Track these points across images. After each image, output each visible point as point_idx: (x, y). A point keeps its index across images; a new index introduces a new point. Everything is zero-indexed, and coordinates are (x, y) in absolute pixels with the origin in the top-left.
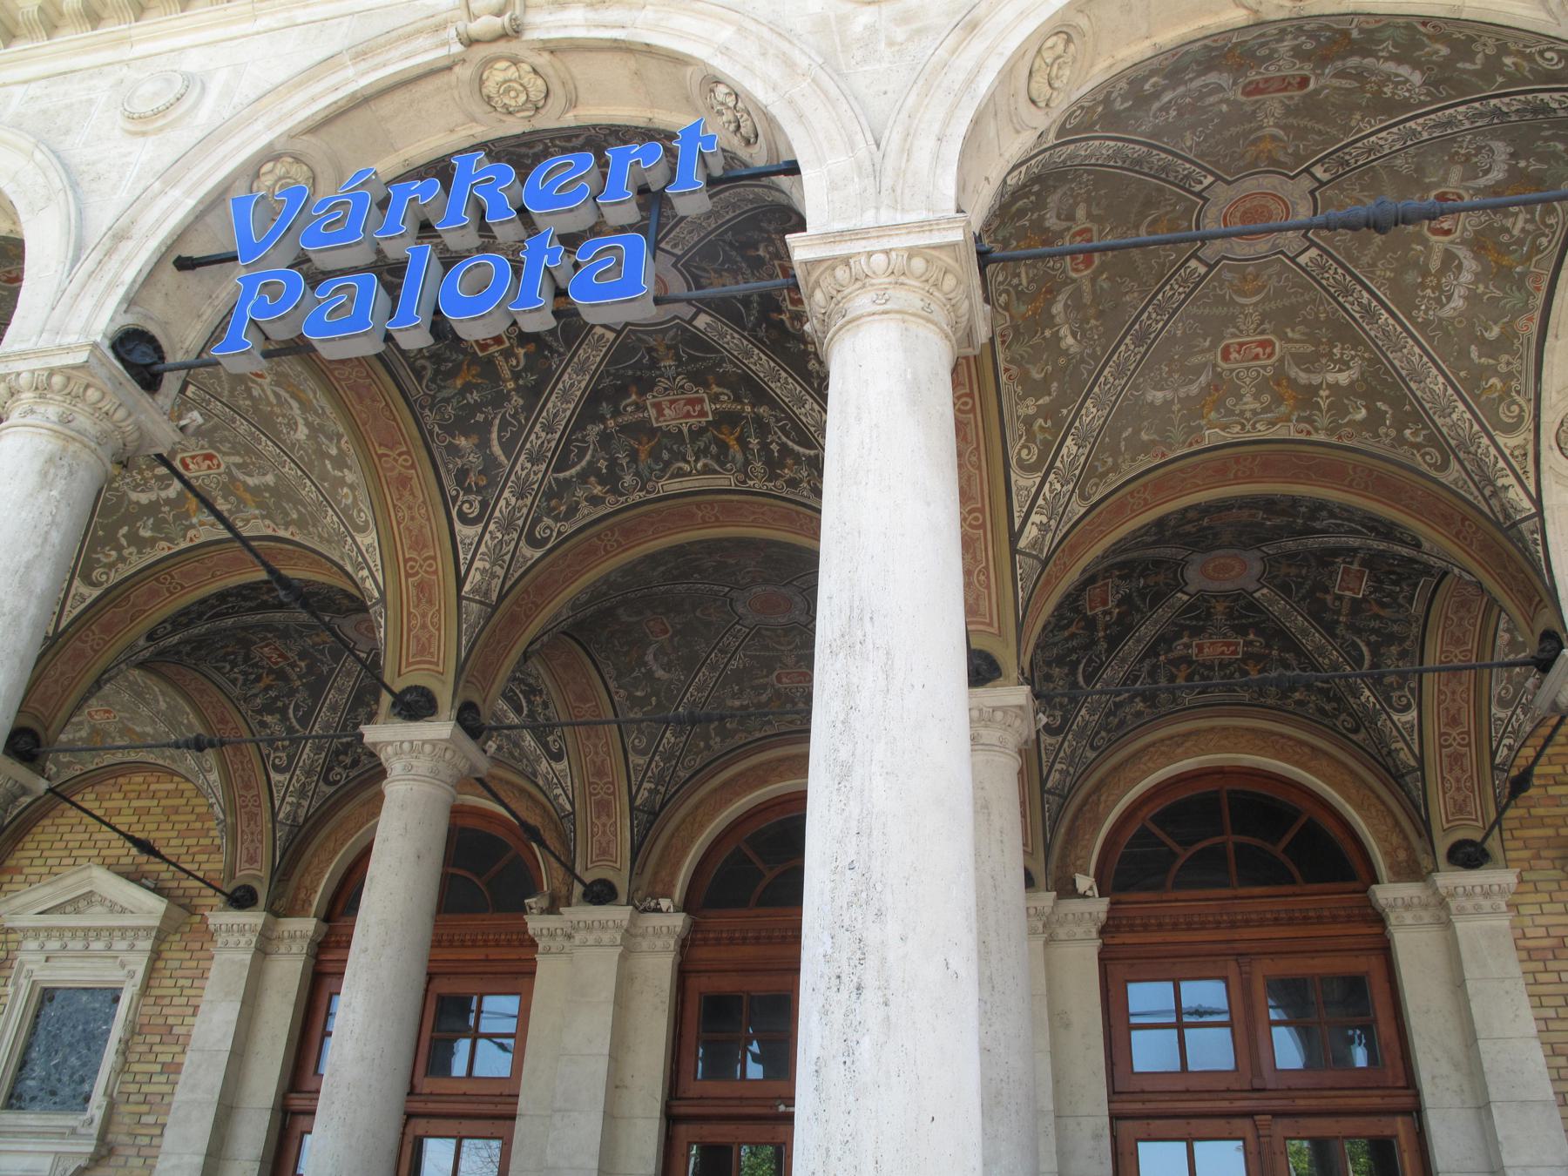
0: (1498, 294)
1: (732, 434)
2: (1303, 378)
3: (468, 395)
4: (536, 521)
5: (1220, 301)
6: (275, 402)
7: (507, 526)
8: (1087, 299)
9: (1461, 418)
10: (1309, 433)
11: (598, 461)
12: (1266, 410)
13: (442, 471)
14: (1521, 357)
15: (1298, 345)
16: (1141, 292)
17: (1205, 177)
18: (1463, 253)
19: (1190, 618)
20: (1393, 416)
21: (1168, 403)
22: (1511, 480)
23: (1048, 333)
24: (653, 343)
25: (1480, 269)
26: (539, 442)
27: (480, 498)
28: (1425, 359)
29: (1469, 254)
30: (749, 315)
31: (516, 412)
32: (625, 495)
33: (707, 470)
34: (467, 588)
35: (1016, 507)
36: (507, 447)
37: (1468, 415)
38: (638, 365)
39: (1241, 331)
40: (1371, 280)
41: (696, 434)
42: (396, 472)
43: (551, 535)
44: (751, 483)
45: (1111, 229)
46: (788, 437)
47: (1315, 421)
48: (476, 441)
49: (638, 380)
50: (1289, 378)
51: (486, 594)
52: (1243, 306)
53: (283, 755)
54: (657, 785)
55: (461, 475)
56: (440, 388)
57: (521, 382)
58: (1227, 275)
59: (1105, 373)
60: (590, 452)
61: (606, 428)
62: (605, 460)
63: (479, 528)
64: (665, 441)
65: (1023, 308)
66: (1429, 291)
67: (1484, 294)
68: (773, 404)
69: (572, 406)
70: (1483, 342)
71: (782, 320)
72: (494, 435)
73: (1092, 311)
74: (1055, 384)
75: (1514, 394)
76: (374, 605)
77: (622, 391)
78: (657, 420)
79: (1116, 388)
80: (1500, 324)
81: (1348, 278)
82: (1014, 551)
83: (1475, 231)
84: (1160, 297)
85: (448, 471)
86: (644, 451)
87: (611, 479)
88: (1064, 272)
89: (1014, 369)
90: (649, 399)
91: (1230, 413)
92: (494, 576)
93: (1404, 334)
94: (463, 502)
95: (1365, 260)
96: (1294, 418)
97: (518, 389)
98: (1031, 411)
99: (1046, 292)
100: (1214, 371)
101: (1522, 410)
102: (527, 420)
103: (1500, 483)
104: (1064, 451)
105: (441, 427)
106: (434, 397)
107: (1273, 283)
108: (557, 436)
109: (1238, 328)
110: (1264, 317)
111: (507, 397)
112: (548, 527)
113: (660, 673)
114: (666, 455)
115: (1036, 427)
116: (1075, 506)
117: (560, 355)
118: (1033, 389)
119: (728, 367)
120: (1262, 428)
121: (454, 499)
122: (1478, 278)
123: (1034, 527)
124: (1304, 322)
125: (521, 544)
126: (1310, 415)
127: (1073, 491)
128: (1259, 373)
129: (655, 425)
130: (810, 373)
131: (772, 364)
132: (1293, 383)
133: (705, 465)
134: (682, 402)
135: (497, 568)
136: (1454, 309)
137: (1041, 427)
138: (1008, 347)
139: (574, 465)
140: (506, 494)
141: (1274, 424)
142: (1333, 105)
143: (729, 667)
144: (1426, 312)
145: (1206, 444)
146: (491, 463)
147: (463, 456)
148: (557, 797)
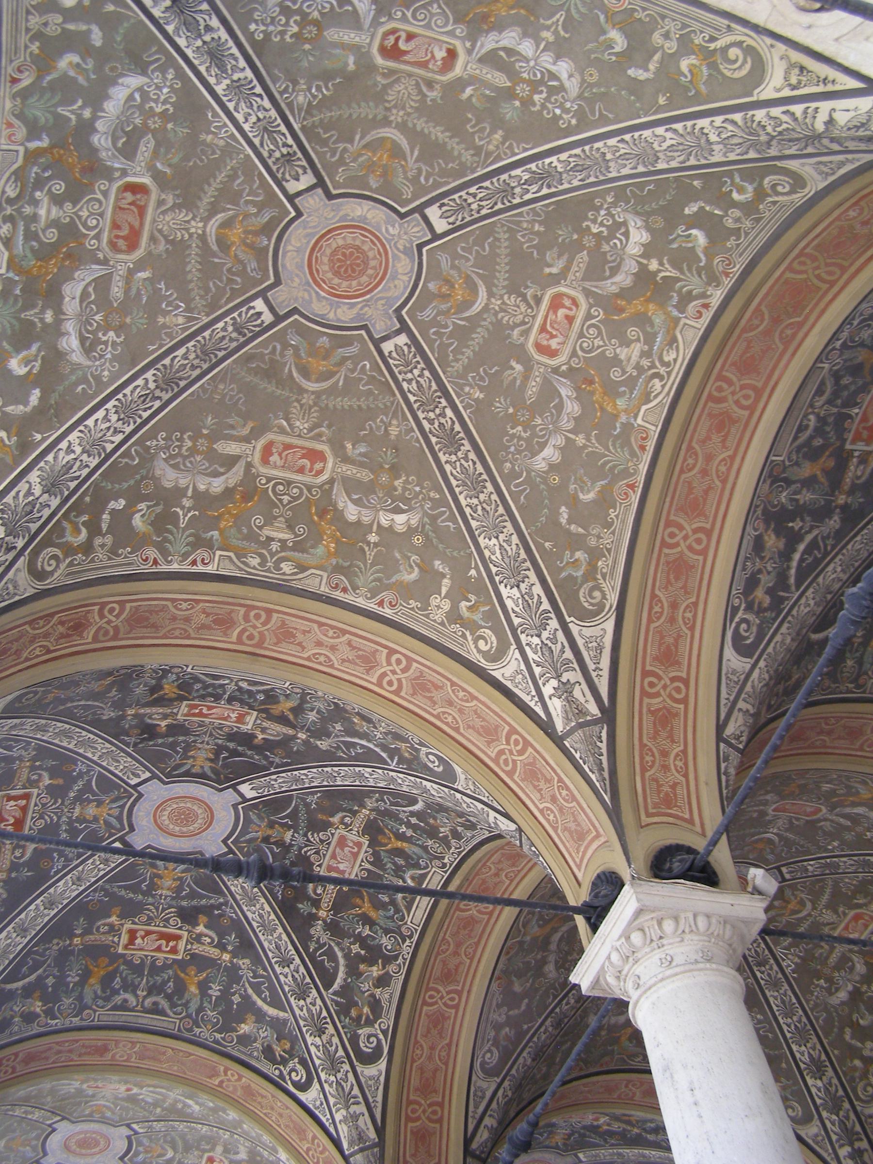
0: (561, 16)
2: (623, 279)
3: (210, 992)
4: (354, 1040)
5: (462, 334)
6: (849, 823)
7: (333, 1065)
8: (365, 475)
9: (720, 130)
10: (706, 306)
12: (650, 339)
13: (254, 1063)
14: (663, 17)
15: (574, 268)
16: (395, 415)
18: (489, 42)
19: (126, 888)
20: (708, 202)
21: (568, 448)
22: (825, 106)
23: (373, 538)
25: (519, 29)
27: (296, 1060)
28: (627, 137)
29: (493, 36)
30: (253, 758)
31: (254, 972)
32: (399, 954)
34: (345, 1145)
35: (526, 698)
36: (275, 1003)
37: (718, 120)
39: (523, 323)
40: (498, 159)
43: (379, 1041)
45: (287, 420)
47: (690, 292)
48: (253, 1018)
50: (617, 296)
52: (486, 308)
54: (851, 1144)
55: (268, 1052)
56: (186, 1005)
57: (230, 948)
58: (428, 314)
59: (463, 503)
60: (336, 949)
61: (324, 921)
63: (316, 1085)
65: (320, 550)
66: (536, 97)
67: (556, 33)
70: (627, 57)
72: (260, 1003)
73: (384, 478)
74: (437, 563)
75: (712, 46)
79: (489, 502)
80: (607, 27)
81: (487, 184)
82: (558, 740)
83: (456, 21)
84: (412, 399)
86: (366, 907)
87: (374, 954)
88: (309, 488)
89: (385, 595)
91: (631, 382)
92: (355, 1117)
93: (587, 148)
94: (290, 1074)
95: (467, 156)
96: (675, 313)
98: (446, 605)
99: (321, 517)
100: (563, 375)
101: (739, 44)
102: (265, 970)
103: (820, 127)
104: (509, 604)
105: (219, 1031)
106: (189, 1016)
107: (468, 267)
108: (297, 960)
109: (516, 325)
110: (514, 289)
111: (235, 968)
112: (369, 1036)
115: (465, 613)
116: (587, 632)
120: (673, 355)
121: (281, 1076)
122: (530, 31)
123: (554, 699)
124: (542, 249)
125: (359, 1069)
126: (679, 292)
128: (593, 325)
132: (623, 293)
134: (338, 850)
135: (353, 1108)
136: (571, 76)
137: (469, 608)
138: (355, 588)
139: (336, 969)
140: (309, 1040)
141: (674, 340)
142: (186, 158)
143: (788, 971)
144: (566, 111)
145: (655, 432)
146: (277, 1025)
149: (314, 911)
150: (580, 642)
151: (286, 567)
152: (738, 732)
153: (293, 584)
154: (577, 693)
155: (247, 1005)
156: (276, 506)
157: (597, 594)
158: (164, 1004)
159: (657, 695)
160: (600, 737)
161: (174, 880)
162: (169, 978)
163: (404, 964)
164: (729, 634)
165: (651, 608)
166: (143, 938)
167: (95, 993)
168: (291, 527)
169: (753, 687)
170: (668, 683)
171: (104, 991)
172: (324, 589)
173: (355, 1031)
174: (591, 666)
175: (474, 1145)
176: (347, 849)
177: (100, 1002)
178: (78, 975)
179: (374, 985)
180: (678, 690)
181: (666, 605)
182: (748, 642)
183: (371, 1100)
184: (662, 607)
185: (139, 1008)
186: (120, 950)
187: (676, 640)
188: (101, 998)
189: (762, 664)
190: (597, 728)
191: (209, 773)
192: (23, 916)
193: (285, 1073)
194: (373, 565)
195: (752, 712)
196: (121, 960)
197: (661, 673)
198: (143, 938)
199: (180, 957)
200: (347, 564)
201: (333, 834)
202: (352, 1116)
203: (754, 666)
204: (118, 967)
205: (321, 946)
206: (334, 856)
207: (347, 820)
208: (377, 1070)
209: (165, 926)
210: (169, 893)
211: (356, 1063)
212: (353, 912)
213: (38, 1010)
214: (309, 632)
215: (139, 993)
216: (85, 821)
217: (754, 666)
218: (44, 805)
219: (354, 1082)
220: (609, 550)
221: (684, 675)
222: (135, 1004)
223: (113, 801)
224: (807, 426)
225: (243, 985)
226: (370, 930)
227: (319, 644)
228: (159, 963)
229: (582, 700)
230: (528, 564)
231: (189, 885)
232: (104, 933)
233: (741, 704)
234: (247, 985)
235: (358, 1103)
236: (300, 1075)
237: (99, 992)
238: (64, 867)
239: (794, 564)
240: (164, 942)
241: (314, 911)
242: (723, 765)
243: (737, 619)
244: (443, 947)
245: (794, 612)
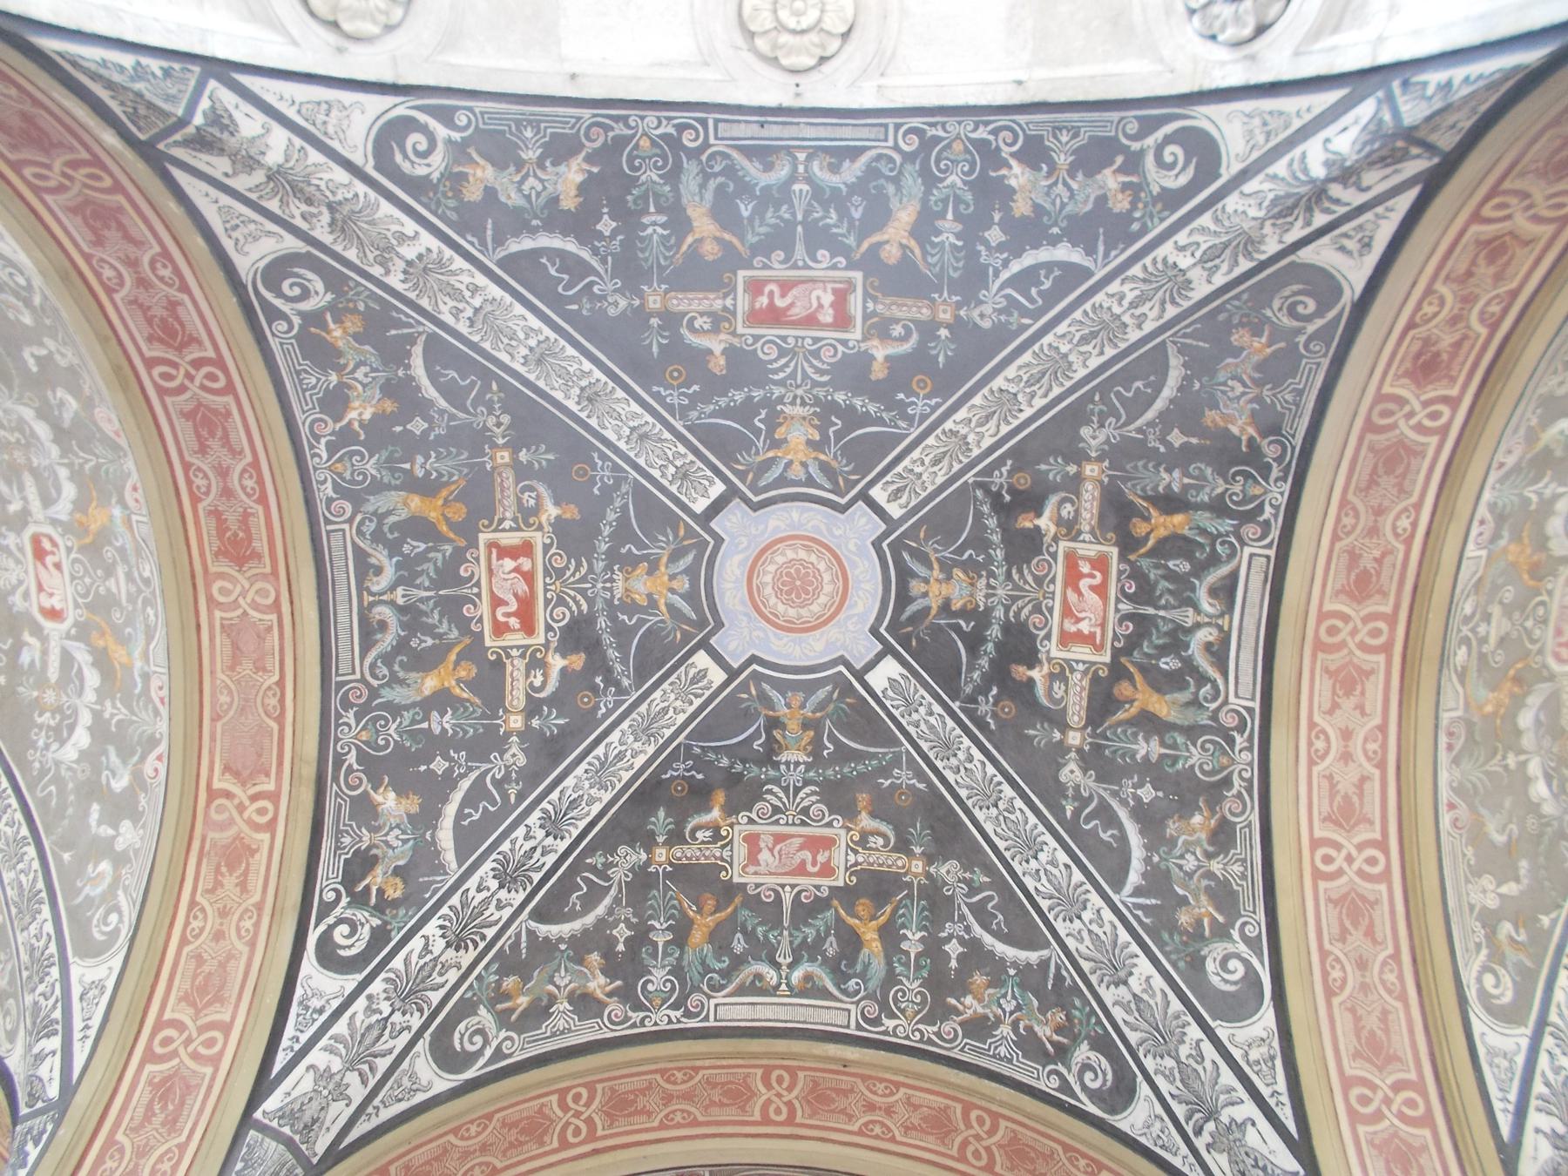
1: (873, 918)
3: (435, 715)
4: (466, 1008)
24: (782, 711)
26: (528, 846)
27: (376, 922)
30: (971, 669)
31: (507, 778)
33: (810, 989)
34: (272, 1103)
36: (467, 839)
38: (741, 752)
41: (806, 910)
42: (232, 832)
43: (480, 1052)
46: (985, 926)
48: (415, 809)
49: (732, 780)
51: (308, 1128)
56: (394, 680)
57: (535, 723)
60: (607, 901)
61: (649, 862)
62: (629, 926)
63: (350, 982)
64: (745, 913)
68: (971, 856)
69: (607, 797)
71: (1031, 681)
72: (451, 809)
77: (699, 795)
78: (851, 285)
86: (703, 924)
88: (1540, 652)
89: (1463, 811)
90: (740, 828)
92: (340, 1093)
94: (340, 921)
97: (526, 734)
98: (1492, 903)
102: (521, 797)
105: (362, 757)
106: (374, 693)
108: (562, 846)
112: (481, 1032)
114: (739, 944)
117: (621, 691)
118: (1496, 862)
119: (904, 776)
121: (326, 909)
130: (1061, 789)
131: (991, 770)
133: (808, 978)
134: (797, 842)
135: (352, 1078)
139: (573, 916)
140: (431, 928)
146: (425, 858)
147: (376, 830)
149: (661, 839)
151: (1462, 653)
153: (1445, 671)
155: (434, 792)
156: (1523, 611)
158: (387, 641)
161: (649, 596)
162: (440, 636)
163: (634, 1026)
164: (402, 107)
166: (517, 570)
167: (389, 513)
168: (1502, 641)
171: (394, 527)
172: (1445, 717)
173: (480, 1001)
177: (370, 527)
178: (428, 474)
179: (572, 992)
183: (376, 1102)
185: (368, 599)
186: (483, 538)
188: (380, 524)
191: (911, 609)
192: (570, 351)
193: (338, 911)
194: (1487, 773)
196: (462, 543)
198: (517, 570)
199: (488, 642)
200: (1478, 738)
201: (829, 824)
202: (339, 1085)
204: (449, 541)
205: (1086, 802)
206: (779, 838)
208: (431, 1078)
209: (547, 602)
210: (618, 593)
211: (427, 1035)
212: (686, 903)
213: (353, 415)
214: (1363, 714)
215: (400, 591)
216: (772, 427)
218: (816, 354)
219: (396, 1052)
222: (375, 589)
223: (825, 468)
225: (470, 769)
226: (667, 943)
227: (1347, 735)
228: (467, 610)
231: (642, 622)
232: (519, 500)
234: (473, 775)
235: (364, 1082)
236: (350, 944)
237: (392, 519)
238: (670, 409)
240: (513, 607)
241: (661, 839)
244: (679, 1075)
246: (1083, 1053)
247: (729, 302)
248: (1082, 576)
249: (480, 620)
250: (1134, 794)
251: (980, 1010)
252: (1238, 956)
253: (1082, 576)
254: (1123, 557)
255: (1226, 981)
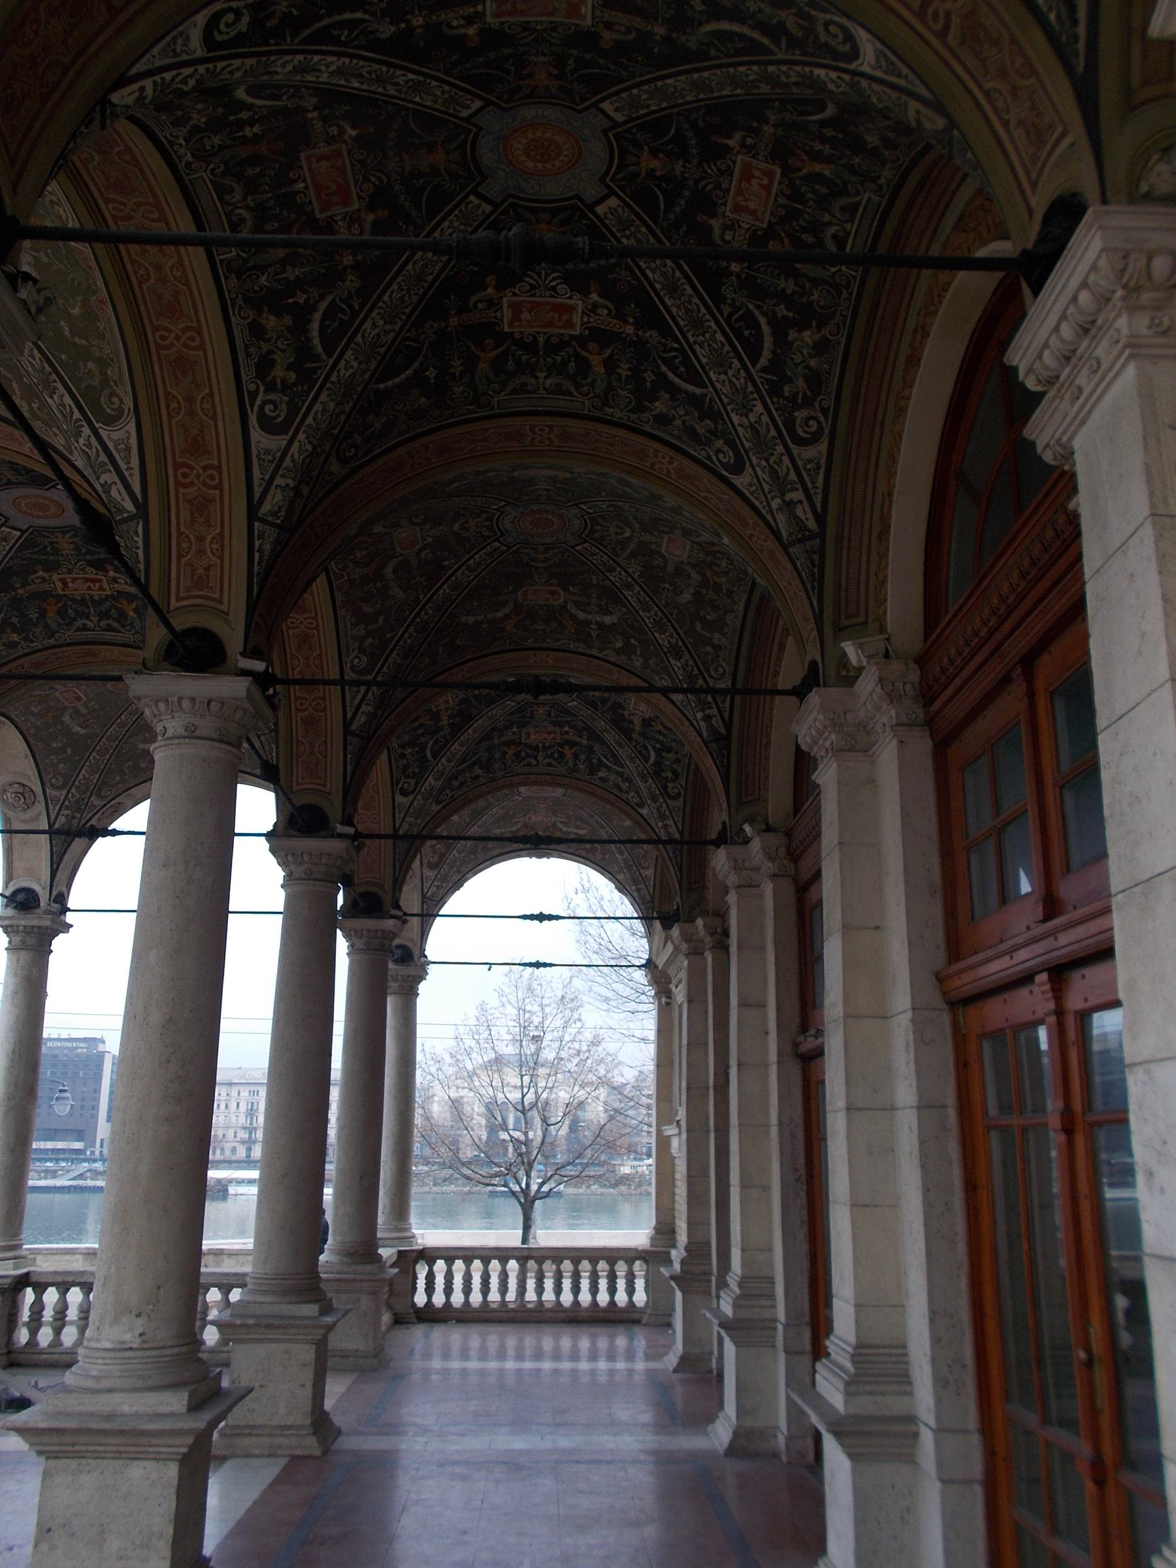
11: (427, 370)
17: (473, 101)
34: (785, 536)
36: (693, 377)
42: (175, 349)
43: (819, 423)
44: (610, 411)
53: (632, 794)
60: (757, 313)
61: (738, 276)
76: (124, 520)
85: (248, 355)
92: (74, 817)
94: (264, 403)
98: (363, 633)
102: (362, 306)
105: (632, 411)
113: (608, 620)
116: (116, 436)
121: (253, 395)
127: (95, 432)
129: (506, 329)
148: (107, 487)
150: (111, 445)
152: (276, 508)
154: (114, 493)
157: (115, 399)
159: (192, 484)
160: (136, 532)
164: (253, 419)
165: (168, 406)
169: (293, 461)
170: (201, 471)
174: (123, 466)
175: (354, 727)
176: (754, 181)
180: (212, 477)
181: (181, 400)
182: (279, 420)
184: (178, 402)
187: (201, 431)
189: (301, 436)
190: (133, 524)
193: (712, 454)
195: (292, 485)
197: (192, 463)
199: (578, 333)
203: (291, 442)
205: (736, 309)
207: (749, 141)
211: (791, 446)
217: (291, 442)
220: (112, 360)
221: (215, 462)
224: (558, 385)
229: (119, 498)
230: (54, 376)
233: (279, 481)
239: (315, 333)
242: (257, 543)
243: (258, 403)
245: (333, 378)
246: (719, 443)
247: (480, 8)
248: (752, 177)
249: (310, 203)
250: (773, 311)
251: (664, 410)
252: (815, 419)
253: (752, 177)
254: (783, 175)
255: (805, 432)
